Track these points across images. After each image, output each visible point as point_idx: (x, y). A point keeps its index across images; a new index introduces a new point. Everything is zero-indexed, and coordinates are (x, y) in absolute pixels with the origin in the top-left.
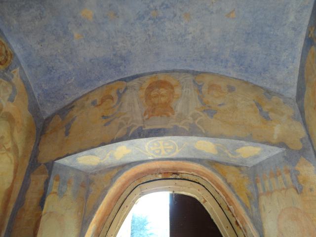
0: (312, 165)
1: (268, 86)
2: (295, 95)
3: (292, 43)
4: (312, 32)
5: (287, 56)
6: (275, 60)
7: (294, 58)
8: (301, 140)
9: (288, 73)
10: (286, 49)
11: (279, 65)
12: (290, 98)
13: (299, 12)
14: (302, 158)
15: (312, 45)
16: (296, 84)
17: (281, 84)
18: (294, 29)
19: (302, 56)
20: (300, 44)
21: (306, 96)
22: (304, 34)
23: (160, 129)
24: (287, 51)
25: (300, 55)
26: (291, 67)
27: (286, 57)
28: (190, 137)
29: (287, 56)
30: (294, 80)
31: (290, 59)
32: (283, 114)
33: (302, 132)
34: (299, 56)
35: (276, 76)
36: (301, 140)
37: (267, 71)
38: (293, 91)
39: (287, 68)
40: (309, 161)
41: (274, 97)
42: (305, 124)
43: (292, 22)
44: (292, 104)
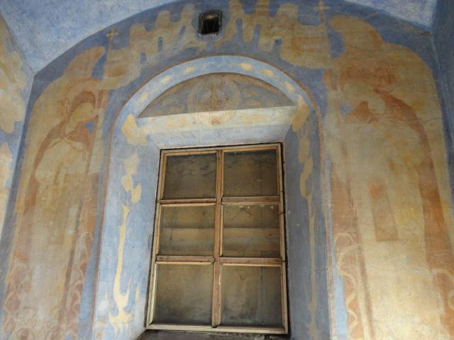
0: (11, 156)
1: (17, 34)
2: (40, 70)
3: (86, 22)
4: (112, 34)
5: (70, 27)
6: (55, 18)
7: (74, 36)
8: (16, 123)
9: (54, 43)
10: (76, 22)
11: (53, 26)
12: (31, 69)
13: (119, 6)
14: (6, 144)
15: (103, 45)
16: (50, 61)
17: (36, 46)
18: (101, 13)
19: (82, 42)
20: (92, 31)
21: (57, 81)
22: (104, 26)
23: (451, 140)
24: (75, 23)
25: (81, 39)
26: (63, 41)
27: (67, 27)
28: (164, 118)
29: (70, 27)
30: (52, 55)
31: (69, 33)
32: (13, 81)
33: (21, 116)
34: (80, 38)
35: (39, 33)
36: (16, 123)
37: (35, 18)
38: (41, 65)
39: (58, 38)
40: (11, 151)
41: (15, 52)
42: (30, 108)
43: (105, 6)
44: (29, 77)
